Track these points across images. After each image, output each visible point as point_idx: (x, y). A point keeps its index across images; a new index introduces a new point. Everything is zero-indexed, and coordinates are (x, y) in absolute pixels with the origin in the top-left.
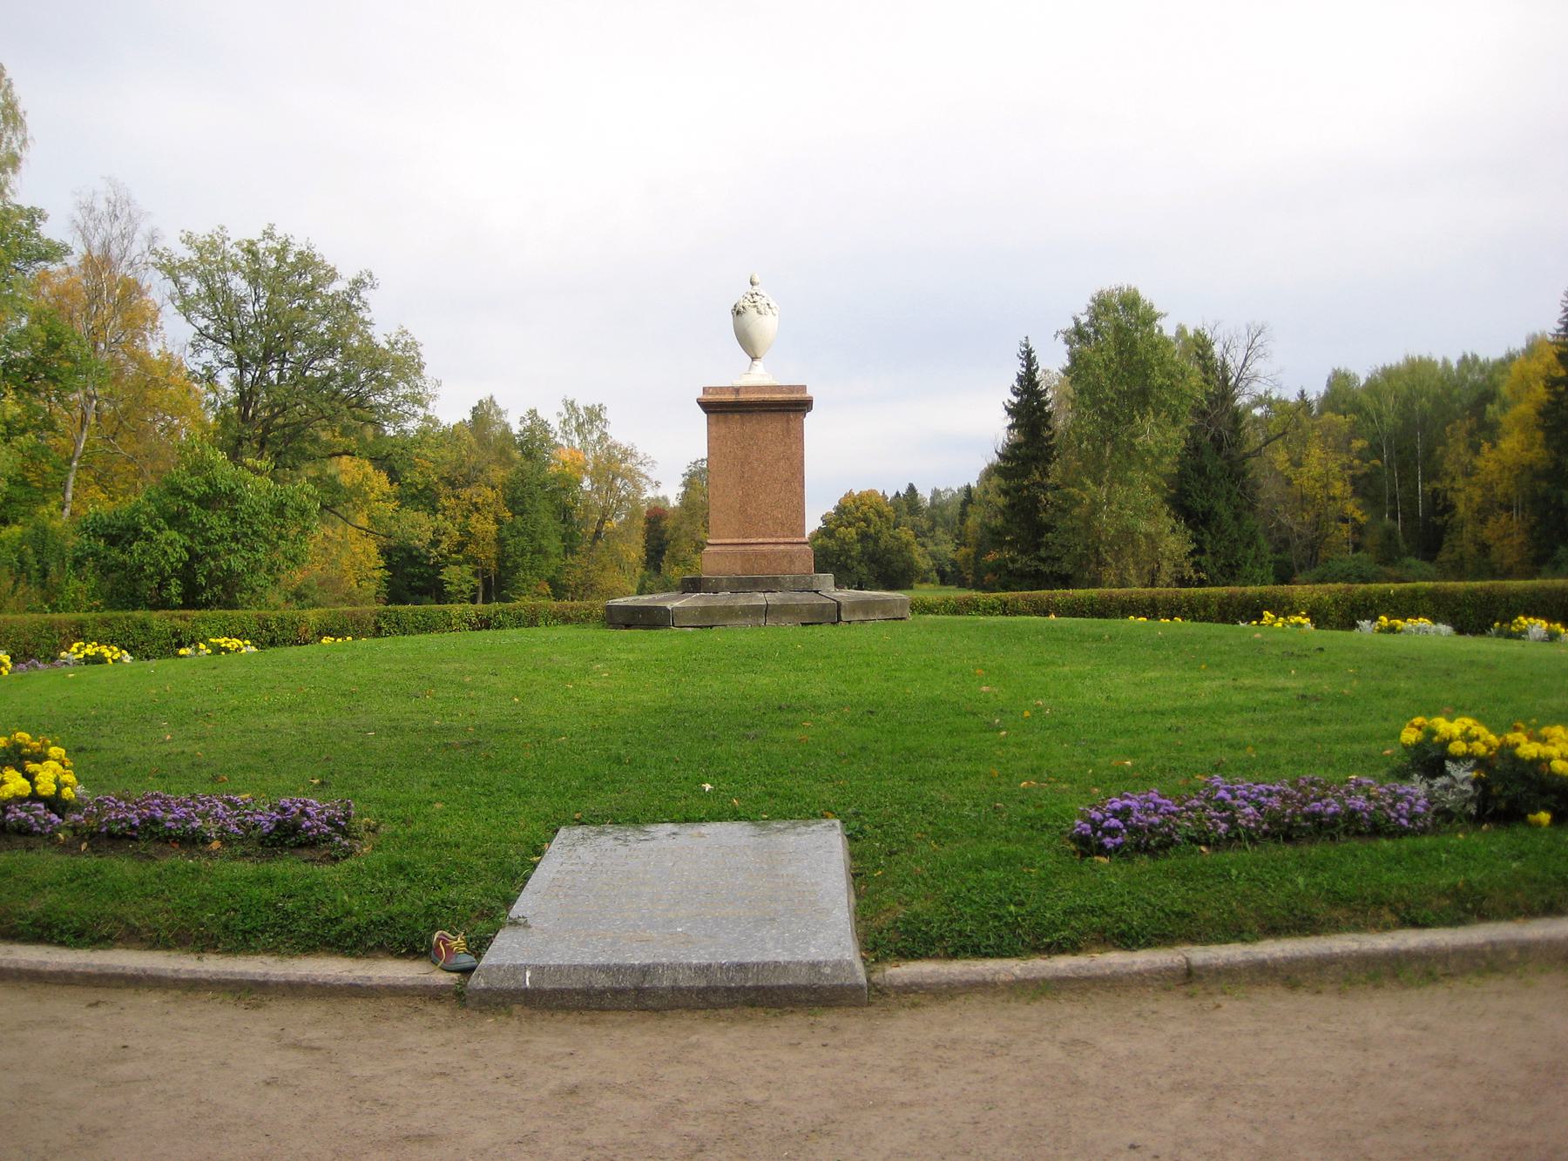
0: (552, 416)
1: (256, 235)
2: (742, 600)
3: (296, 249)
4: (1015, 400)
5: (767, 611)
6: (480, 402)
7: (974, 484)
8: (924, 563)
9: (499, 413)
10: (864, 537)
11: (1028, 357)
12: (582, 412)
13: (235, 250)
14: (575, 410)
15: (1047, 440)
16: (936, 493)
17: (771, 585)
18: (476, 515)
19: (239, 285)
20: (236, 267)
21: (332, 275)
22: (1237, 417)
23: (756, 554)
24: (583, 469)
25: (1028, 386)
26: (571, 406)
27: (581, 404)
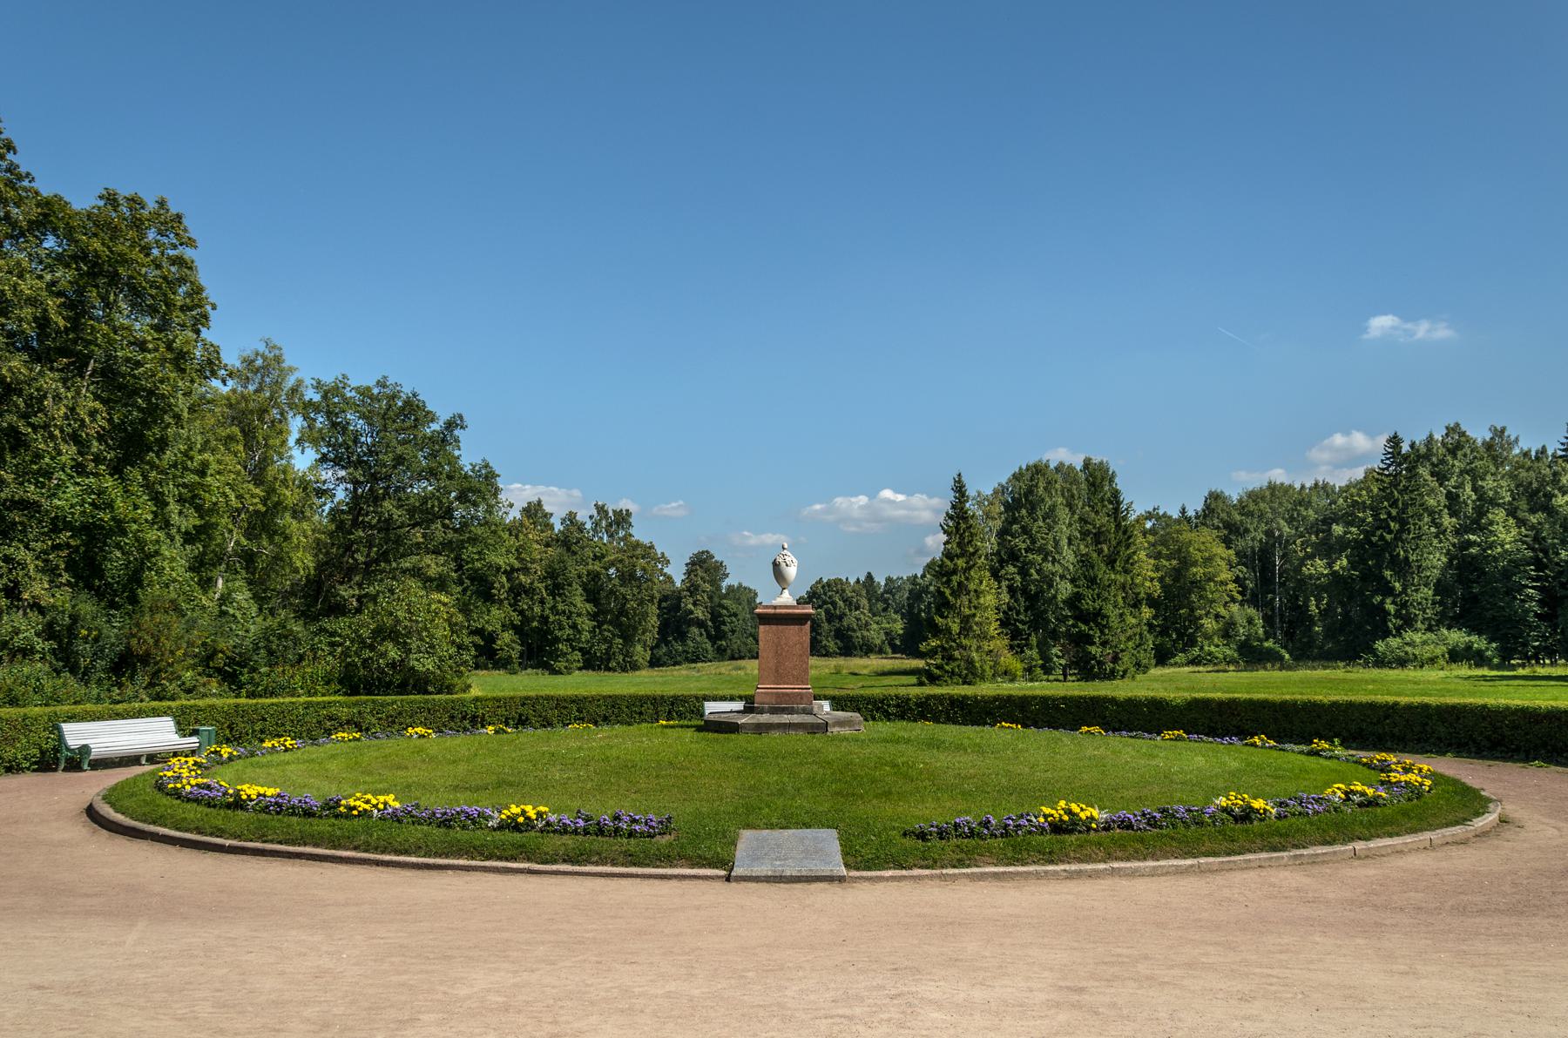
1: (371, 383)
2: (776, 719)
11: (960, 488)
13: (353, 394)
16: (889, 580)
17: (791, 711)
21: (432, 418)
26: (601, 509)
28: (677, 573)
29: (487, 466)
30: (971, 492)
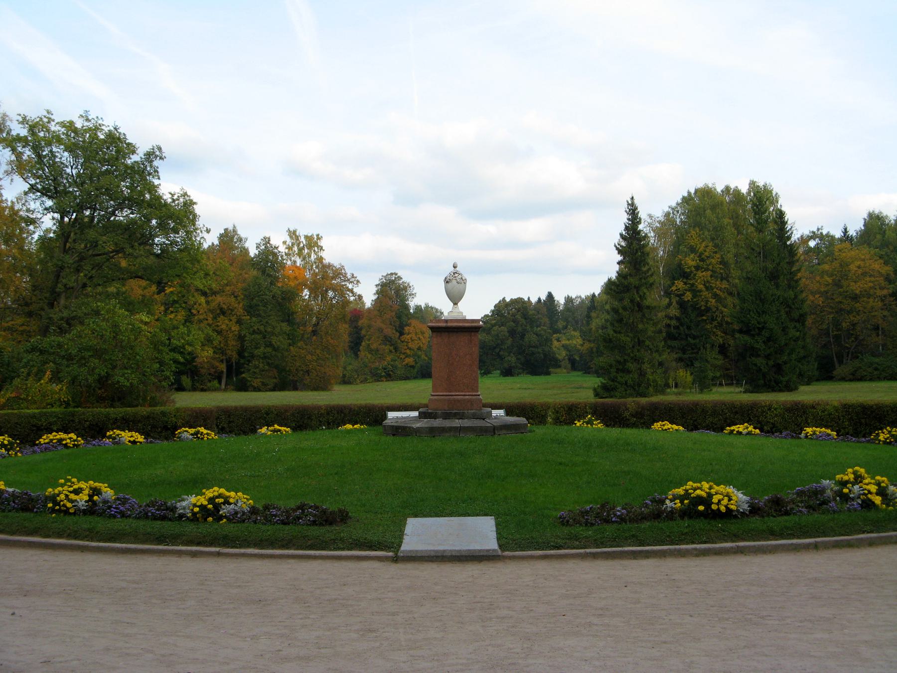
0: (280, 241)
2: (448, 423)
3: (106, 129)
5: (460, 429)
6: (226, 230)
7: (596, 294)
8: (562, 354)
9: (240, 240)
10: (512, 333)
11: (633, 211)
12: (302, 239)
13: (58, 128)
14: (297, 238)
15: (645, 273)
17: (461, 416)
19: (64, 156)
20: (59, 141)
22: (791, 250)
23: (455, 400)
26: (293, 234)
27: (302, 232)
28: (367, 293)
30: (643, 214)
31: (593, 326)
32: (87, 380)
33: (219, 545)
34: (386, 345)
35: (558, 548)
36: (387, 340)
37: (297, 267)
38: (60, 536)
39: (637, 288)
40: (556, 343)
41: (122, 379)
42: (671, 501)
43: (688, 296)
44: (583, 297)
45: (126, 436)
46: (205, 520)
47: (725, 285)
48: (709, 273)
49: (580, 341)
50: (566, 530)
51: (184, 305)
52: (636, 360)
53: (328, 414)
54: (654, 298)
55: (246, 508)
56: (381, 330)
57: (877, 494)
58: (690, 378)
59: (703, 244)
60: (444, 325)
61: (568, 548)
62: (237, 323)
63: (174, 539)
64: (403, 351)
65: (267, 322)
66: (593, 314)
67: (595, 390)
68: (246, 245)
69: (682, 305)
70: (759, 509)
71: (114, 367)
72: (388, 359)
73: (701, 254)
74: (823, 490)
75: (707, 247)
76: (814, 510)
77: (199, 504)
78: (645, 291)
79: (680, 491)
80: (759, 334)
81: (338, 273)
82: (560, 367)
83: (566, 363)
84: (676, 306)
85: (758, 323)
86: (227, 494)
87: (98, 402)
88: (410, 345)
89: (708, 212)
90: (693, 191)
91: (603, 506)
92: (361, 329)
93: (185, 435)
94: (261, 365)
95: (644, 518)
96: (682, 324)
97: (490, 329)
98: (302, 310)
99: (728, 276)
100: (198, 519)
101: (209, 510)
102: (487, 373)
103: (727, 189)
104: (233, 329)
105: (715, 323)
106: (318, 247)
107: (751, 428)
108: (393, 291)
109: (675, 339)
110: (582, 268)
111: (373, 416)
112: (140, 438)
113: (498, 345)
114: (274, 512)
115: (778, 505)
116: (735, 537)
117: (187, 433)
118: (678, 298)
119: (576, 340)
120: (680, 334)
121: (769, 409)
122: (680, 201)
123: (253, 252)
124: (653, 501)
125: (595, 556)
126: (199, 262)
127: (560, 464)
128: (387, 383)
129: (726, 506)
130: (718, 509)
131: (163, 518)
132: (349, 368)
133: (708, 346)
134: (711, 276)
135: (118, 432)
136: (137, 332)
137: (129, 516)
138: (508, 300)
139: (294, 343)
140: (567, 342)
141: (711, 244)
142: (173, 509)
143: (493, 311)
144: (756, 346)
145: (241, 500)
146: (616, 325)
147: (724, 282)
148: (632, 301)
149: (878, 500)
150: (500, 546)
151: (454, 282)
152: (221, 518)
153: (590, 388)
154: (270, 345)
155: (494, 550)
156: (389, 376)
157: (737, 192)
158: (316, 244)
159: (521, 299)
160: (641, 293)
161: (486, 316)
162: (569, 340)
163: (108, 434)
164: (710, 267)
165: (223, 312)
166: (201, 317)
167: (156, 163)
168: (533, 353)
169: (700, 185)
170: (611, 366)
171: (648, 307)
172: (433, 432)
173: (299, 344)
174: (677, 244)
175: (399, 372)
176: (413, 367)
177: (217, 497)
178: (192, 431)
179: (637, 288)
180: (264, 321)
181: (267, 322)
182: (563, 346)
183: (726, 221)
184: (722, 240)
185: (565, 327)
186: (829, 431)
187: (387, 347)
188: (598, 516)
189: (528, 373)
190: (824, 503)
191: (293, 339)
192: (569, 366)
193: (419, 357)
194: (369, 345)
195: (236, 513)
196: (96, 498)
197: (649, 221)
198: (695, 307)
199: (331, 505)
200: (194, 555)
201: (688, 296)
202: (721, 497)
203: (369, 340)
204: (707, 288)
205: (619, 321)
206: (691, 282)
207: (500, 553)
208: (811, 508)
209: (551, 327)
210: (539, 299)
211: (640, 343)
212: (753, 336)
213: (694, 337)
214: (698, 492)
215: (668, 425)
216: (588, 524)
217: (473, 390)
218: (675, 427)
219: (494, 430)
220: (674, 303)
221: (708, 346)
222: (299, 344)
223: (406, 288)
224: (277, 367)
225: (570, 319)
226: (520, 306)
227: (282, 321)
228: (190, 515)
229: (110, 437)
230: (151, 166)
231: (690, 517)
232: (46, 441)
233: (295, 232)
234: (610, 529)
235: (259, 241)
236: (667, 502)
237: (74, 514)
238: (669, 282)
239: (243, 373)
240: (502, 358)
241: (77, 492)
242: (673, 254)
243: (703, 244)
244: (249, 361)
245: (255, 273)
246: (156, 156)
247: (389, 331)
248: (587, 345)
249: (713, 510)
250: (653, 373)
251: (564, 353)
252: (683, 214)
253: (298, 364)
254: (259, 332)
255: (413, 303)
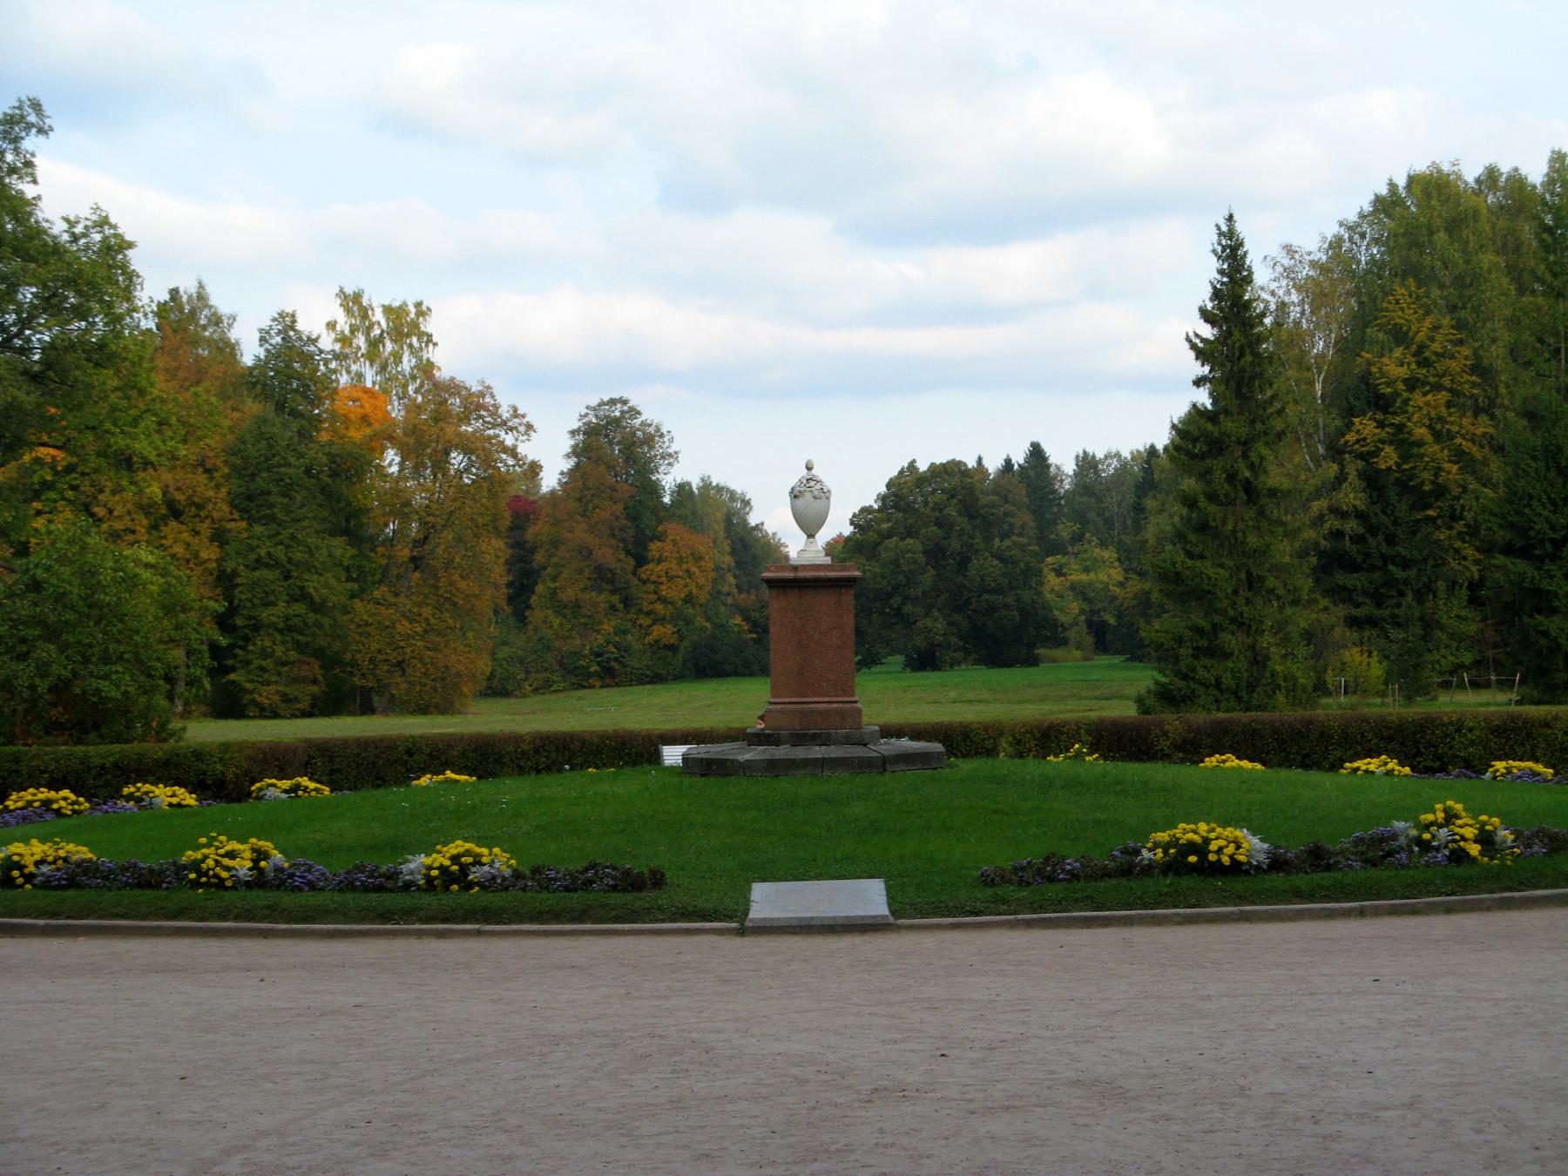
0: (319, 319)
2: (800, 753)
4: (1207, 331)
5: (823, 763)
7: (1160, 447)
8: (1070, 611)
9: (216, 320)
10: (936, 554)
11: (1232, 252)
12: (378, 316)
14: (364, 313)
17: (824, 740)
18: (173, 524)
23: (812, 711)
24: (388, 437)
25: (1231, 303)
26: (353, 302)
27: (378, 298)
28: (550, 455)
29: (103, 222)
31: (1150, 533)
32: (32, 687)
33: (477, 921)
34: (600, 591)
35: (977, 914)
36: (603, 577)
37: (366, 391)
38: (224, 918)
39: (1246, 444)
40: (1052, 580)
41: (104, 685)
42: (1150, 850)
43: (1389, 457)
44: (1126, 454)
45: (163, 794)
46: (447, 888)
47: (1484, 426)
48: (1444, 396)
49: (1117, 574)
50: (989, 892)
51: (70, 494)
52: (1240, 623)
53: (537, 751)
54: (1292, 467)
55: (507, 872)
56: (585, 552)
57: (1475, 842)
58: (1377, 670)
59: (1427, 323)
60: (790, 575)
61: (991, 914)
62: (212, 540)
63: (407, 915)
64: (646, 607)
65: (293, 537)
66: (1150, 503)
67: (1140, 701)
68: (233, 335)
69: (1373, 480)
70: (1286, 862)
71: (86, 661)
72: (607, 627)
73: (1422, 347)
74: (1394, 836)
75: (1436, 328)
76: (1374, 865)
77: (437, 864)
78: (1264, 451)
79: (1163, 836)
80: (1554, 557)
81: (476, 404)
82: (1064, 642)
83: (1079, 633)
84: (1357, 482)
85: (1553, 528)
86: (478, 850)
87: (48, 733)
88: (664, 591)
89: (1442, 236)
90: (1401, 182)
91: (1047, 859)
92: (533, 550)
93: (271, 792)
94: (279, 650)
95: (1106, 874)
96: (1373, 530)
97: (876, 546)
98: (383, 505)
99: (1492, 404)
100: (435, 888)
101: (453, 873)
102: (869, 661)
103: (1491, 174)
104: (204, 555)
105: (1460, 526)
106: (421, 335)
107: (1393, 764)
108: (616, 448)
109: (1352, 567)
110: (1111, 388)
111: (637, 751)
112: (191, 800)
113: (897, 587)
114: (552, 874)
115: (1317, 857)
116: (1241, 899)
117: (275, 788)
118: (1361, 464)
119: (1107, 572)
120: (1368, 555)
121: (1459, 730)
122: (1368, 208)
123: (250, 352)
124: (1125, 852)
125: (1029, 924)
126: (142, 392)
127: (995, 812)
128: (605, 692)
129: (1231, 857)
130: (1219, 860)
131: (380, 889)
132: (504, 652)
133: (1441, 585)
134: (1449, 405)
135: (148, 787)
136: (131, 582)
137: (322, 889)
138: (923, 467)
139: (362, 590)
140: (1084, 577)
141: (1446, 321)
142: (394, 875)
143: (883, 498)
144: (1545, 585)
145: (498, 860)
146: (1192, 537)
147: (1483, 418)
148: (1231, 477)
149: (1474, 849)
150: (893, 912)
151: (808, 496)
152: (470, 885)
153: (1128, 698)
154: (303, 596)
155: (883, 917)
156: (610, 672)
157: (1517, 182)
158: (415, 326)
159: (959, 463)
160: (1254, 458)
161: (865, 510)
162: (1087, 570)
163: (126, 791)
164: (1446, 382)
165: (175, 512)
166: (118, 525)
167: (30, 143)
168: (992, 609)
169: (1421, 166)
170: (1180, 640)
171: (1273, 493)
172: (774, 768)
173: (377, 594)
174: (1362, 320)
175: (634, 663)
176: (672, 648)
177: (463, 855)
178: (285, 784)
179: (1246, 444)
180: (286, 533)
181: (293, 537)
182: (1073, 587)
183: (1487, 259)
184: (1476, 310)
185: (1078, 538)
186: (1539, 768)
187: (604, 596)
188: (1039, 872)
189: (978, 662)
190: (1390, 854)
191: (360, 578)
192: (1090, 640)
193: (688, 623)
194: (554, 592)
195: (494, 878)
196: (263, 864)
197: (1287, 262)
198: (1405, 486)
199: (640, 866)
200: (441, 935)
201: (1389, 457)
202: (1223, 843)
203: (554, 579)
204: (1437, 436)
205: (1200, 529)
206: (1397, 420)
207: (892, 920)
208: (1373, 863)
209: (1041, 538)
210: (1008, 462)
211: (1253, 582)
212: (1541, 560)
213: (1406, 564)
214: (1190, 836)
215: (1232, 762)
216: (1023, 883)
217: (845, 693)
218: (1246, 764)
219: (883, 764)
220: (1352, 476)
221: (1441, 585)
222: (377, 594)
223: (651, 437)
224: (318, 653)
225: (1091, 515)
226: (955, 481)
227: (333, 534)
228: (422, 882)
229: (130, 797)
230: (17, 151)
231: (1177, 873)
232: (20, 804)
233: (357, 297)
234: (1053, 890)
235: (265, 323)
236: (1145, 853)
237: (234, 887)
238: (1338, 423)
239: (233, 669)
240: (908, 622)
241: (232, 855)
242: (1347, 348)
243: (1427, 323)
244: (246, 639)
245: (253, 407)
246: (29, 126)
247: (610, 555)
248: (1136, 585)
249: (1211, 863)
250: (1285, 657)
251: (1075, 606)
252: (1376, 241)
253: (375, 646)
254: (275, 564)
255: (669, 479)
